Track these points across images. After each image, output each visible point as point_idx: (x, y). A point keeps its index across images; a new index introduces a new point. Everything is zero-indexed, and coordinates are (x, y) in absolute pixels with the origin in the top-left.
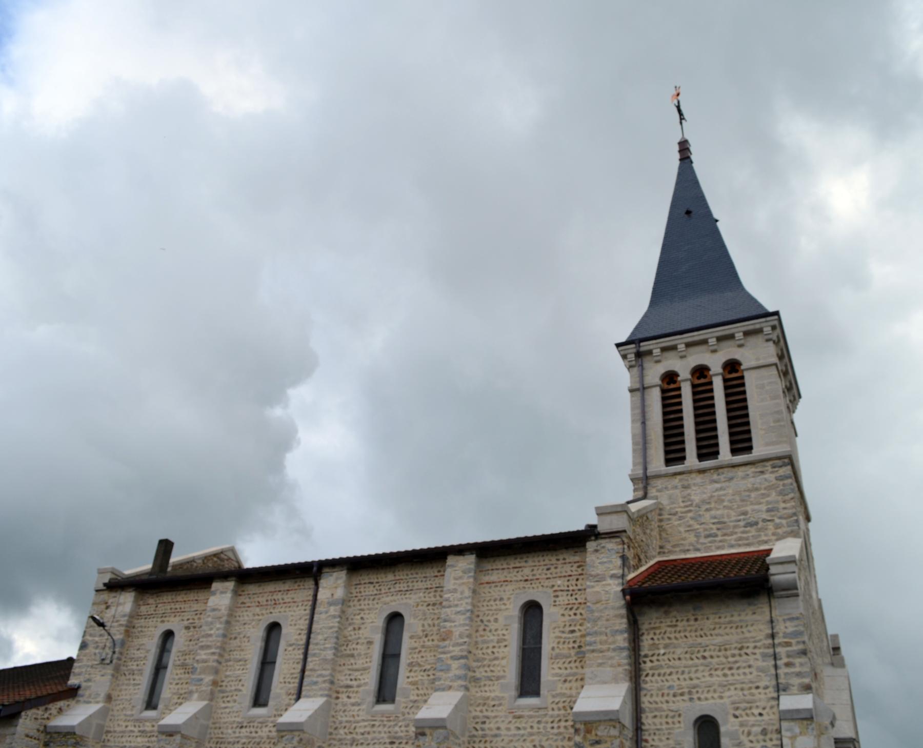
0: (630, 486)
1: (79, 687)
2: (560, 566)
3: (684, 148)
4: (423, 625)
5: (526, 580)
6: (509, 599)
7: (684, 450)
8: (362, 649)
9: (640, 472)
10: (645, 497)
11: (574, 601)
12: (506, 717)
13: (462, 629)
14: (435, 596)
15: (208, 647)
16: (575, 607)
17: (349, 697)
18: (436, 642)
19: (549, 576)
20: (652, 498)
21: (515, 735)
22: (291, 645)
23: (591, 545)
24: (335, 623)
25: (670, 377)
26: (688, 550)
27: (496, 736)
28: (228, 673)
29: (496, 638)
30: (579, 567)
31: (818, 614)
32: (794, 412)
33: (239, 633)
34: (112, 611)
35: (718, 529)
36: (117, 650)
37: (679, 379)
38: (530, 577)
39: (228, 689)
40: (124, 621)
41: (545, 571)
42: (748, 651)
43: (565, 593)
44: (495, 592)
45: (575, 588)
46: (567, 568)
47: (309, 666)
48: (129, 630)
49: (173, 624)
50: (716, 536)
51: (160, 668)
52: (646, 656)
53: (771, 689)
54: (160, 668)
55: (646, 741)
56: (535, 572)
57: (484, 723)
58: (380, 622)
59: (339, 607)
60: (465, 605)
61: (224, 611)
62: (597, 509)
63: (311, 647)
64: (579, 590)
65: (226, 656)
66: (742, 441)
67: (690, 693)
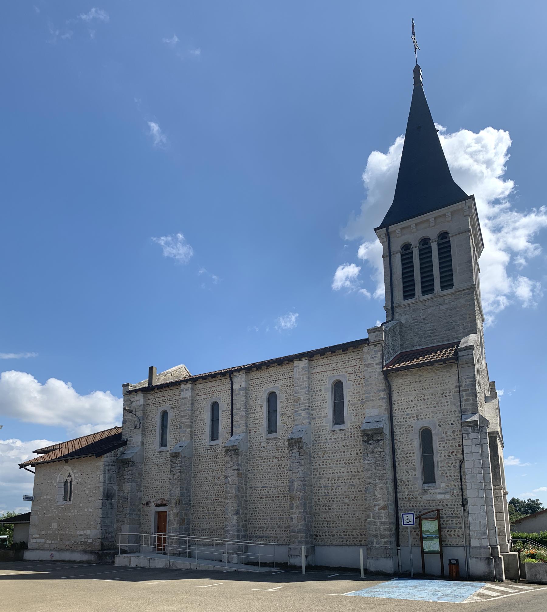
1: (127, 440)
3: (416, 71)
4: (286, 396)
7: (414, 290)
8: (258, 409)
9: (458, 384)
10: (392, 320)
12: (329, 434)
13: (304, 396)
14: (290, 382)
15: (185, 416)
16: (359, 380)
17: (255, 432)
18: (293, 403)
20: (396, 320)
21: (334, 442)
22: (224, 411)
23: (366, 349)
24: (243, 399)
25: (407, 247)
26: (416, 346)
27: (325, 442)
28: (197, 426)
29: (321, 399)
31: (485, 372)
32: (479, 258)
33: (198, 408)
34: (134, 404)
36: (141, 422)
37: (412, 247)
38: (336, 368)
39: (199, 433)
40: (141, 408)
42: (447, 395)
44: (319, 377)
45: (358, 371)
47: (235, 419)
48: (193, 402)
49: (166, 406)
51: (164, 427)
52: (394, 401)
53: (457, 412)
54: (164, 427)
55: (396, 440)
57: (319, 437)
58: (265, 397)
59: (244, 392)
60: (305, 384)
61: (189, 399)
62: (368, 330)
63: (234, 411)
65: (195, 419)
66: (447, 282)
67: (417, 416)
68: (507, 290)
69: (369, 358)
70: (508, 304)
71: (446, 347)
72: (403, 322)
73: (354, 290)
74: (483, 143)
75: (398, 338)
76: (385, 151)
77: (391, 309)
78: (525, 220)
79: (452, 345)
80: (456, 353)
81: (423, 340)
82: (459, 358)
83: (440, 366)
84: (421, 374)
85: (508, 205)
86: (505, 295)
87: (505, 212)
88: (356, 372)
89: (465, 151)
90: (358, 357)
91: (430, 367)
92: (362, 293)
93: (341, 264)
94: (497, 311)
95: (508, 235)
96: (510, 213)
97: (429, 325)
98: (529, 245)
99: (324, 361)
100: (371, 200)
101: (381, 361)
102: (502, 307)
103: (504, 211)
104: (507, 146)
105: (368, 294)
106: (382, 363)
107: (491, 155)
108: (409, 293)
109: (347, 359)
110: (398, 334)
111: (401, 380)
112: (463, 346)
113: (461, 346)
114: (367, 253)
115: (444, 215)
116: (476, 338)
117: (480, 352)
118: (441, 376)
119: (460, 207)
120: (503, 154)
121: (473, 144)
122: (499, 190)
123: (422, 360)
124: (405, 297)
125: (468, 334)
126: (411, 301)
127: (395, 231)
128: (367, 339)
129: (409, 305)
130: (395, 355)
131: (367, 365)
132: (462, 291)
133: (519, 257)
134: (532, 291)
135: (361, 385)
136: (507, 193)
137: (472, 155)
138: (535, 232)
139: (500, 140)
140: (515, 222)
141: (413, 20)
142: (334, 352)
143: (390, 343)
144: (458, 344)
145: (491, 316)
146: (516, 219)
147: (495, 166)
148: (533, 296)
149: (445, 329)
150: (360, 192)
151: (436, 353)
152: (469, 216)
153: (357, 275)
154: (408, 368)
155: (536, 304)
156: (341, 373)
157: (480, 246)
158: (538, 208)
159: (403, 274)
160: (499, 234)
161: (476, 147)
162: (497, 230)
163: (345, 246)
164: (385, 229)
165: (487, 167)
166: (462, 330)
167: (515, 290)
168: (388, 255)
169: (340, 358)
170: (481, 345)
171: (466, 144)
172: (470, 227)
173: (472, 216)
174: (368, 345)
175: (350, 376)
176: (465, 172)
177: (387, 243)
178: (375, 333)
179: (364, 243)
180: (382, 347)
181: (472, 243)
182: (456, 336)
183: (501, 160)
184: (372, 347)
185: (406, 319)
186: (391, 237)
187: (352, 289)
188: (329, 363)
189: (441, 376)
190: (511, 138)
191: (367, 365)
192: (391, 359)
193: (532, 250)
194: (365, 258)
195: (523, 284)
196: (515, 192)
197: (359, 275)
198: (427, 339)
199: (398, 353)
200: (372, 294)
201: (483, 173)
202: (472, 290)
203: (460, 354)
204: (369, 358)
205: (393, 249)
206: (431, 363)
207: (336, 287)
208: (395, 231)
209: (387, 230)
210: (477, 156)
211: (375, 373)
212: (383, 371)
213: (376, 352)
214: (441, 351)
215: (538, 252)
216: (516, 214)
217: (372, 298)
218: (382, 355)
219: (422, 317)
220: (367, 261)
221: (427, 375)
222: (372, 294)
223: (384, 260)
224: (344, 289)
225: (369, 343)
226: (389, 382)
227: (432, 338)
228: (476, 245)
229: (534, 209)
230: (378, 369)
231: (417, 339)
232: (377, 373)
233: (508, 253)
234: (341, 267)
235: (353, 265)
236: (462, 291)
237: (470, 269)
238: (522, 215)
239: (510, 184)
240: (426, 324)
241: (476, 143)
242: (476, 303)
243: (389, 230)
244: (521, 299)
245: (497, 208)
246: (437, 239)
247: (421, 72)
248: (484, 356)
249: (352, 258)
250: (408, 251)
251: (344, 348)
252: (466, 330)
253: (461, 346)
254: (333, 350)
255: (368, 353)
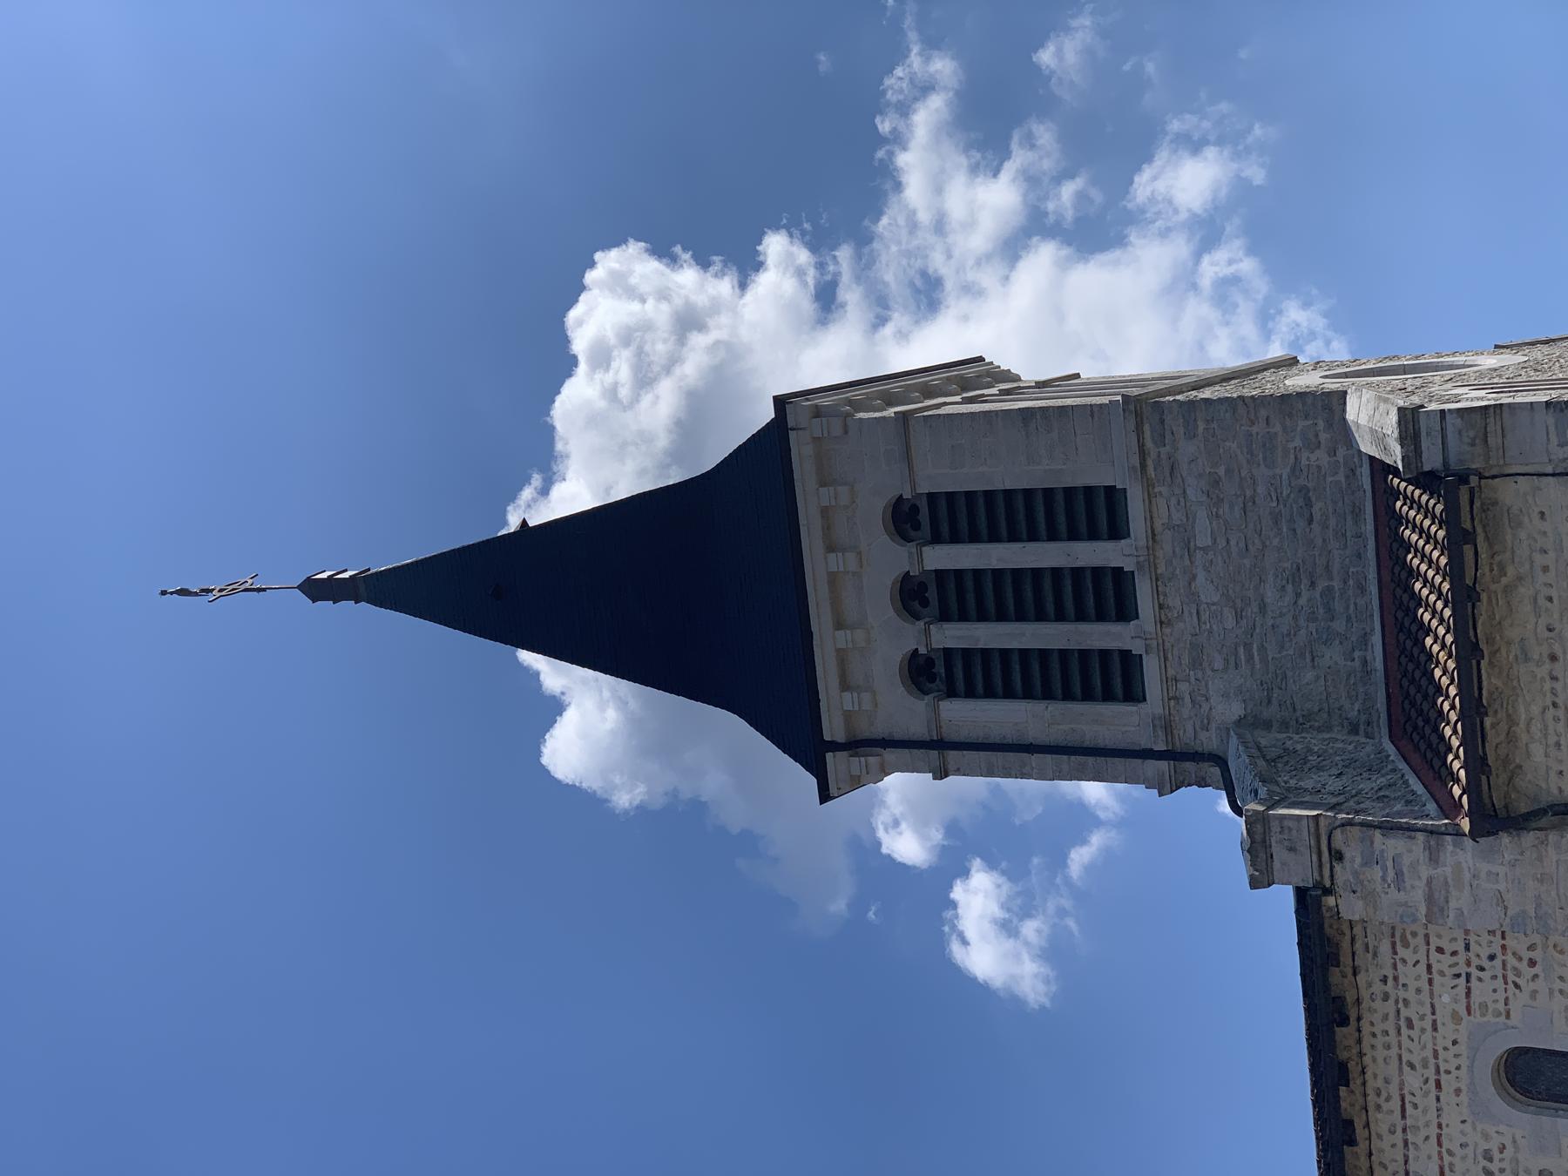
0: (1189, 795)
2: (1402, 994)
3: (316, 590)
5: (1438, 1085)
6: (1486, 1137)
10: (1220, 761)
11: (1498, 962)
16: (1511, 961)
19: (1428, 1024)
23: (1350, 907)
25: (922, 672)
26: (1365, 662)
30: (1406, 945)
31: (1538, 353)
32: (1017, 378)
35: (1313, 584)
37: (923, 650)
41: (1415, 1033)
43: (1474, 983)
45: (1461, 958)
46: (1412, 975)
50: (1329, 589)
56: (1416, 1061)
62: (1255, 884)
64: (1467, 948)
66: (1098, 512)
68: (1178, 248)
69: (1402, 896)
70: (1238, 243)
71: (1389, 522)
72: (1236, 710)
73: (1067, 903)
74: (613, 341)
75: (1315, 741)
76: (554, 708)
77: (1177, 762)
78: (915, 189)
79: (1385, 496)
80: (1428, 481)
81: (1339, 625)
82: (1454, 466)
83: (1483, 556)
84: (1515, 650)
85: (844, 254)
86: (1198, 256)
87: (870, 264)
88: (1463, 969)
89: (625, 409)
90: (1385, 948)
91: (1483, 607)
92: (1089, 869)
93: (941, 944)
94: (1261, 286)
95: (956, 253)
96: (876, 245)
97: (1270, 594)
98: (1010, 169)
99: (1383, 1129)
100: (713, 784)
101: (1420, 836)
102: (1248, 266)
103: (865, 265)
104: (646, 256)
105: (1097, 839)
106: (1431, 832)
107: (659, 313)
108: (1115, 678)
109: (1390, 1006)
110: (1297, 742)
111: (1537, 751)
112: (1397, 450)
113: (1395, 455)
114: (920, 827)
115: (825, 512)
116: (1367, 395)
117: (1437, 377)
118: (1538, 558)
119: (808, 450)
120: (667, 271)
121: (609, 378)
122: (789, 285)
123: (1437, 618)
124: (1132, 693)
125: (1344, 432)
126: (1151, 670)
127: (848, 716)
128: (1301, 893)
129: (1169, 681)
130: (1402, 765)
131: (1436, 907)
132: (1143, 453)
133: (1051, 206)
134: (1195, 146)
135: (1537, 955)
136: (803, 256)
137: (644, 379)
138: (967, 149)
139: (621, 285)
140: (913, 226)
141: (164, 593)
142: (1343, 1067)
143: (1334, 785)
144: (1380, 469)
145: (1280, 312)
146: (901, 221)
147: (701, 300)
148: (1220, 142)
149: (1301, 524)
150: (676, 824)
151: (1414, 574)
152: (848, 415)
153: (1002, 880)
154: (1473, 710)
155: (1258, 131)
156: (1462, 1048)
157: (971, 374)
158: (882, 140)
159: (1028, 695)
160: (949, 285)
161: (622, 369)
162: (928, 295)
163: (871, 915)
164: (829, 756)
165: (701, 327)
166: (1321, 457)
167: (1183, 216)
168: (938, 752)
169: (1380, 1040)
170: (1405, 370)
171: (602, 404)
172: (891, 412)
173: (850, 402)
174: (1328, 892)
175: (1484, 1007)
176: (698, 410)
177: (890, 755)
178: (1276, 850)
179: (873, 831)
180: (1350, 823)
181: (953, 405)
182: (1341, 477)
183: (687, 278)
184: (1343, 874)
185: (1226, 695)
186: (866, 735)
187: (1062, 912)
188: (1396, 1104)
189: (1538, 558)
190: (616, 241)
191: (1436, 907)
192: (1418, 788)
193: (1031, 156)
194: (937, 836)
195: (1161, 186)
196: (807, 226)
197: (1003, 873)
198: (1338, 606)
199: (1390, 749)
200: (1098, 823)
201: (717, 343)
202: (1147, 411)
203: (1431, 460)
204: (1402, 896)
205: (917, 728)
206: (1465, 597)
207: (1041, 988)
208: (848, 716)
209: (835, 746)
210: (654, 363)
211: (1480, 874)
212: (1474, 834)
213: (1371, 860)
214: (1408, 546)
215: (1045, 135)
216: (884, 221)
217: (1119, 824)
218: (1388, 828)
219: (1230, 622)
220: (952, 829)
221: (1522, 620)
222: (1098, 823)
223: (958, 772)
224: (1054, 952)
225: (1318, 884)
226: (1541, 812)
227: (1337, 584)
228: (965, 389)
229: (880, 154)
230: (1463, 857)
231: (1332, 656)
232: (1484, 867)
233: (1026, 247)
234: (956, 948)
235: (958, 892)
236: (1143, 453)
237: (1060, 416)
238: (893, 199)
239: (775, 245)
240: (1263, 608)
241: (607, 369)
242: (1206, 394)
243: (840, 737)
244: (1224, 192)
245: (851, 295)
246: (912, 547)
247: (324, 576)
248: (1460, 359)
249: (928, 894)
250: (940, 668)
251: (1329, 1014)
252: (1323, 437)
253: (1395, 455)
254: (1332, 1074)
255: (1370, 898)
